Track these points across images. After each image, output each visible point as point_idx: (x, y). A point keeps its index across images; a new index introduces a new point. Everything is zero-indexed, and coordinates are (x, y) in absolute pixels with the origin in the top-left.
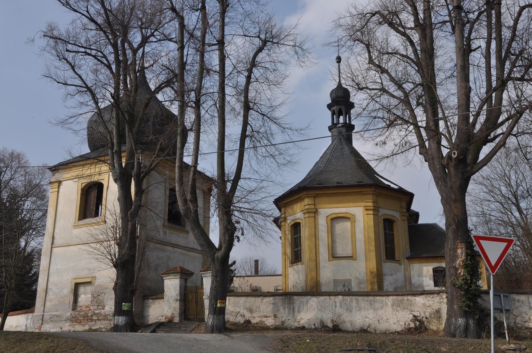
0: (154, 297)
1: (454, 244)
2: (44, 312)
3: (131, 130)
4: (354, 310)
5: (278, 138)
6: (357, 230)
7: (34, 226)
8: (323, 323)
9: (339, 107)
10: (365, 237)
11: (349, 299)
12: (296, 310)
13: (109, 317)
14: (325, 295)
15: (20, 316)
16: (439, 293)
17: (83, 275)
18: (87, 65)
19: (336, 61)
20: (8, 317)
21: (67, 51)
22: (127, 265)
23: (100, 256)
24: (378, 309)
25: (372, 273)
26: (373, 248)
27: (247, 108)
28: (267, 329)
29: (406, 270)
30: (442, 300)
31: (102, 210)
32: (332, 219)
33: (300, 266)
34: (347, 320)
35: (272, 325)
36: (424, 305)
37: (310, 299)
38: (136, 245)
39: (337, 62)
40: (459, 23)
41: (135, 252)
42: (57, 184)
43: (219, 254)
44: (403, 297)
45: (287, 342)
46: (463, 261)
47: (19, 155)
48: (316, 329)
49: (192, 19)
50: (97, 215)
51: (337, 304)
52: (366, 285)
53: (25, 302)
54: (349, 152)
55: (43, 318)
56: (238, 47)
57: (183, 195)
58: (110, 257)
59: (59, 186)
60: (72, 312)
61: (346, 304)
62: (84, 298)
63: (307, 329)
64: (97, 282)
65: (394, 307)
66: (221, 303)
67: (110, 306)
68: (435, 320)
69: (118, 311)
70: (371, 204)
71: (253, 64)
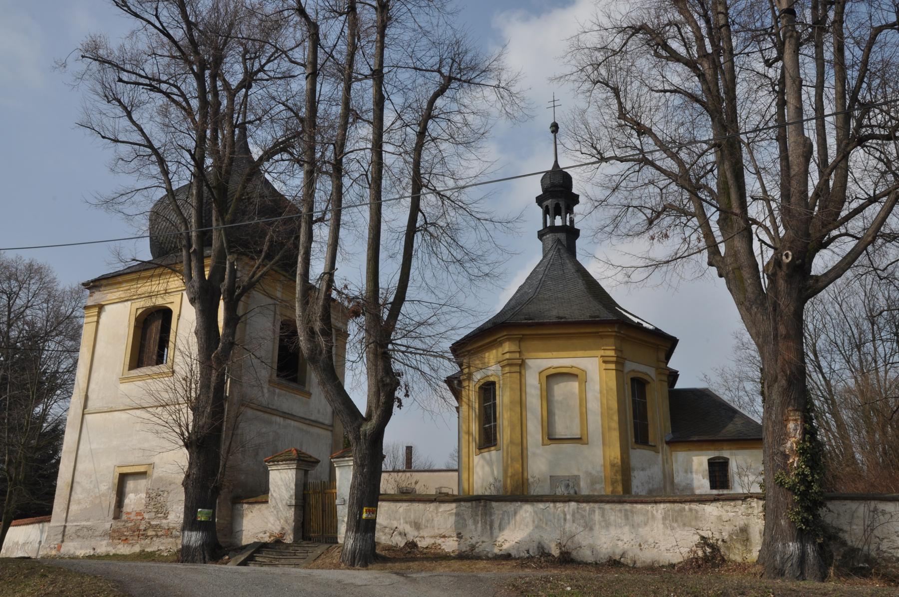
0: (251, 500)
1: (783, 414)
2: (66, 521)
3: (222, 213)
4: (597, 526)
5: (468, 239)
6: (590, 396)
7: (56, 384)
8: (543, 548)
9: (555, 201)
10: (602, 407)
11: (587, 508)
12: (496, 525)
13: (174, 532)
14: (547, 501)
15: (31, 526)
16: (746, 498)
17: (133, 461)
18: (150, 109)
19: (550, 130)
20: (11, 529)
21: (120, 80)
22: (209, 446)
23: (162, 428)
24: (638, 525)
25: (613, 465)
26: (615, 424)
27: (418, 185)
28: (445, 557)
29: (666, 461)
30: (750, 511)
31: (170, 352)
32: (548, 377)
33: (494, 453)
34: (584, 543)
35: (453, 552)
36: (719, 518)
37: (521, 507)
38: (223, 410)
40: (791, 36)
41: (222, 422)
42: (96, 310)
43: (368, 427)
44: (683, 505)
45: (526, 591)
46: (797, 443)
47: (40, 268)
48: (530, 558)
49: (333, 31)
50: (160, 360)
51: (568, 517)
52: (603, 485)
53: (38, 507)
54: (573, 271)
55: (64, 531)
56: (406, 89)
57: (308, 321)
58: (178, 430)
59: (99, 315)
60: (113, 522)
61: (583, 517)
62: (134, 499)
63: (515, 559)
64: (157, 473)
65: (668, 522)
66: (368, 511)
67: (176, 514)
68: (738, 545)
69: (191, 523)
70: (612, 353)
71: (429, 115)
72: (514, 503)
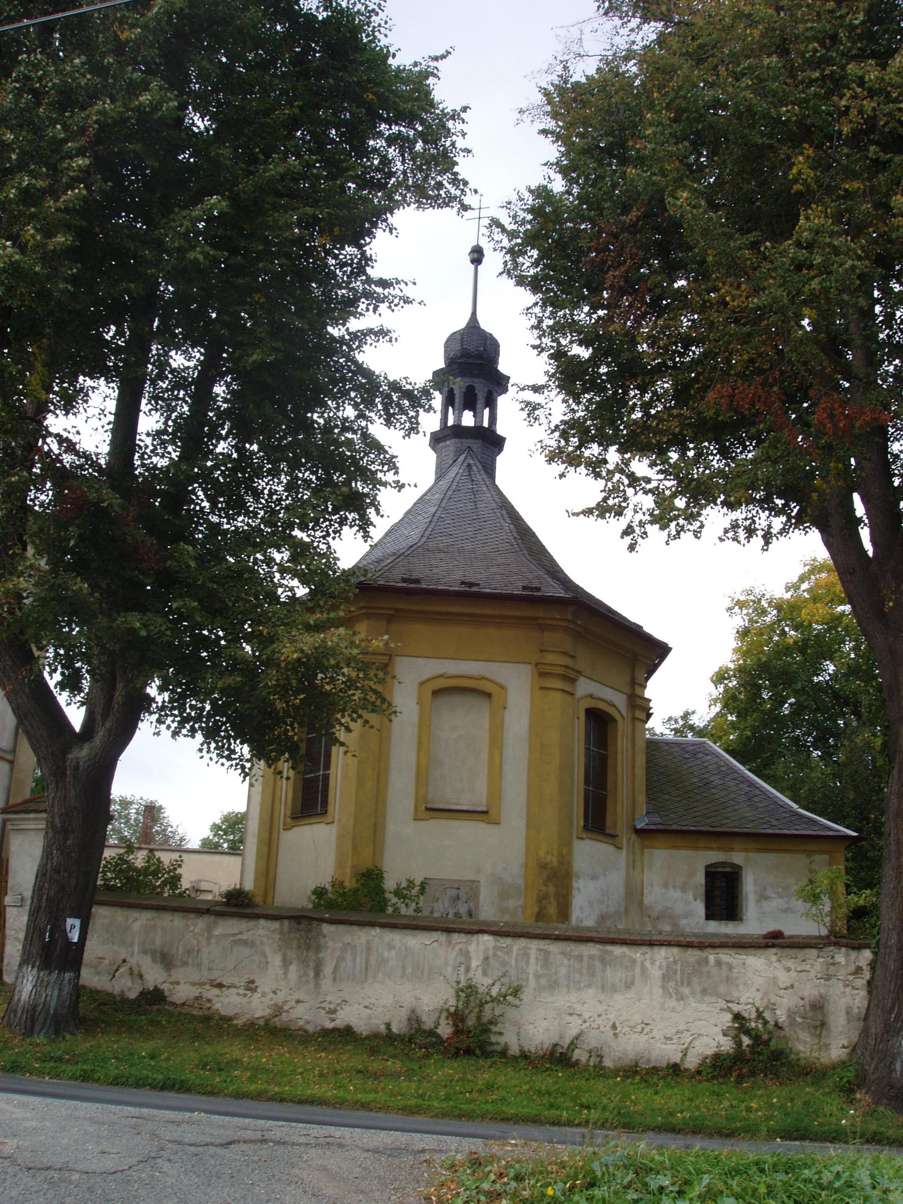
9: (468, 381)
12: (328, 970)
19: (468, 259)
24: (614, 989)
39: (473, 262)
51: (474, 964)
65: (672, 984)
72: (367, 929)
